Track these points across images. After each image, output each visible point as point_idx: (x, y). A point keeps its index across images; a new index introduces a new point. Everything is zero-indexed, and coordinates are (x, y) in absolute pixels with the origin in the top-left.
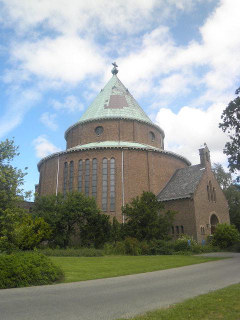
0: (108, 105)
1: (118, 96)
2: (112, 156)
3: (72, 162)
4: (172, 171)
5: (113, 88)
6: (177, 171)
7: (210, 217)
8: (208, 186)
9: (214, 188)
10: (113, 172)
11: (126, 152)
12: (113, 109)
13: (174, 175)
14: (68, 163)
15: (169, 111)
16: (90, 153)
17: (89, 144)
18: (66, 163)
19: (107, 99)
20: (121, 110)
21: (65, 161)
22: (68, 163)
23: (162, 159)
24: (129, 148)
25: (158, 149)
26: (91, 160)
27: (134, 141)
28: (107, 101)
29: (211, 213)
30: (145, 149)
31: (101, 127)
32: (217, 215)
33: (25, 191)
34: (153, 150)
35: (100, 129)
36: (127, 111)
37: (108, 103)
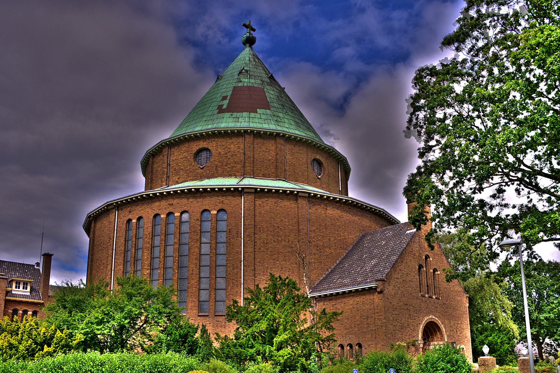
0: (225, 107)
1: (250, 88)
2: (220, 206)
3: (139, 219)
4: (352, 237)
5: (240, 73)
6: (364, 236)
7: (421, 327)
8: (420, 267)
9: (435, 270)
10: (222, 237)
11: (251, 197)
12: (235, 114)
13: (356, 245)
14: (134, 221)
15: (533, 135)
16: (175, 201)
17: (215, 179)
18: (129, 221)
19: (225, 95)
20: (252, 115)
21: (155, 212)
22: (134, 221)
23: (328, 212)
24: (256, 189)
25: (338, 196)
26: (177, 214)
27: (277, 178)
28: (224, 98)
29: (426, 319)
30: (292, 192)
31: (207, 149)
32: (439, 322)
33: (511, 215)
34: (310, 194)
35: (204, 154)
36: (263, 117)
37: (226, 103)
